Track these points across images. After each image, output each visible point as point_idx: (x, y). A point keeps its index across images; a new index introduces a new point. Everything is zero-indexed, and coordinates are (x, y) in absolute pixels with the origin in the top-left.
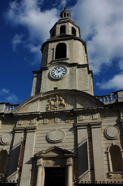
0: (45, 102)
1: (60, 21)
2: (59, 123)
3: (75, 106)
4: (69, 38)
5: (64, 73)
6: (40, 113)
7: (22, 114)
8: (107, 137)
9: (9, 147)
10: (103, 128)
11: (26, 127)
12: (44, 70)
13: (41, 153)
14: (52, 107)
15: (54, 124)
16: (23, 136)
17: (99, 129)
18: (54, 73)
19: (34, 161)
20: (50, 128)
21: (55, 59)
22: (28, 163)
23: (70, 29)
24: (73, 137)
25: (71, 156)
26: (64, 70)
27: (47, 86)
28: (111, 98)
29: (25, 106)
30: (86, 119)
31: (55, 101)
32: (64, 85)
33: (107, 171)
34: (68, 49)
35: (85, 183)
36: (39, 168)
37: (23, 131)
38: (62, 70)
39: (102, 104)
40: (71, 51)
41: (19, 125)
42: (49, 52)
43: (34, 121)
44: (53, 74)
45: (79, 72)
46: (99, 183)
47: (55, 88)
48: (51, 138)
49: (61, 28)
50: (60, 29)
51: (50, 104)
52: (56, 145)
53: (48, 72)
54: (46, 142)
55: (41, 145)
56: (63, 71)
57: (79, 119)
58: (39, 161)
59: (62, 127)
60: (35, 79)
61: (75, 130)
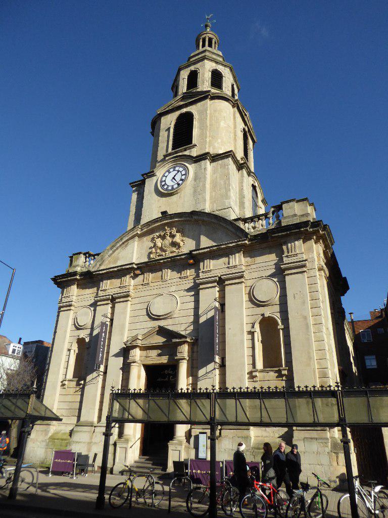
0: (147, 242)
1: (191, 60)
2: (169, 282)
3: (198, 243)
4: (205, 96)
5: (183, 177)
6: (136, 265)
7: (209, 250)
8: (255, 302)
9: (277, 308)
10: (249, 283)
11: (221, 275)
12: (148, 178)
13: (135, 338)
14: (158, 251)
15: (161, 283)
16: (217, 295)
17: (239, 286)
18: (165, 181)
19: (125, 352)
20: (155, 292)
21: (173, 149)
22: (117, 355)
23: (208, 76)
24: (192, 305)
25: (184, 342)
26: (183, 172)
27: (153, 208)
28: (269, 218)
29: (111, 254)
30: (215, 267)
31: (163, 238)
32: (180, 204)
33: (248, 368)
34: (195, 123)
35: (239, 391)
36: (132, 367)
37: (216, 284)
38: (178, 172)
39: (245, 234)
40: (203, 127)
41: (206, 272)
42: (160, 138)
43: (128, 280)
44: (163, 183)
45: (214, 171)
46: (239, 391)
47: (162, 213)
48: (155, 311)
49: (189, 77)
50: (188, 80)
51: (155, 245)
52: (162, 323)
53: (155, 179)
54: (147, 318)
55: (138, 326)
56: (182, 175)
57: (288, 252)
58: (132, 352)
59: (173, 289)
60: (134, 196)
61: (195, 289)
